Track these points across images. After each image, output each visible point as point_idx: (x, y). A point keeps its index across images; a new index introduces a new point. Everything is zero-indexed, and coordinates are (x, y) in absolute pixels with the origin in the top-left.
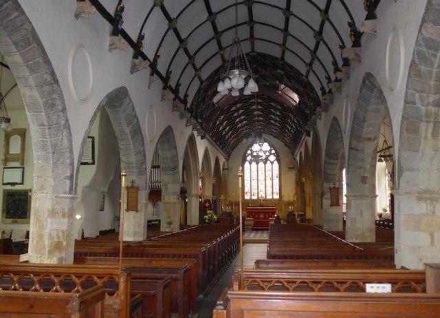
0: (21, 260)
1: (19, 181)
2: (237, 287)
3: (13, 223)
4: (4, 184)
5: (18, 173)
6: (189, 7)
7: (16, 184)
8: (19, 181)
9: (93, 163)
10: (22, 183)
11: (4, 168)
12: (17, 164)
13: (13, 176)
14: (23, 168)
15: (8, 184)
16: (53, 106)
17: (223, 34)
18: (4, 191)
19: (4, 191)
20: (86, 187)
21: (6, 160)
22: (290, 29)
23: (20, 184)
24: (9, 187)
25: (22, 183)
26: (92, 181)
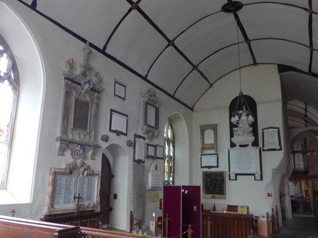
0: (266, 235)
1: (215, 165)
2: (302, 210)
3: (213, 197)
4: (202, 167)
5: (214, 158)
6: (296, 5)
7: (213, 167)
8: (215, 165)
9: (280, 149)
10: (217, 167)
11: (201, 155)
12: (213, 152)
13: (209, 161)
14: (217, 155)
15: (205, 167)
16: (93, 90)
17: (247, 45)
18: (203, 172)
19: (203, 172)
20: (275, 169)
21: (203, 148)
22: (309, 50)
23: (215, 167)
24: (206, 170)
25: (217, 167)
26: (280, 164)
